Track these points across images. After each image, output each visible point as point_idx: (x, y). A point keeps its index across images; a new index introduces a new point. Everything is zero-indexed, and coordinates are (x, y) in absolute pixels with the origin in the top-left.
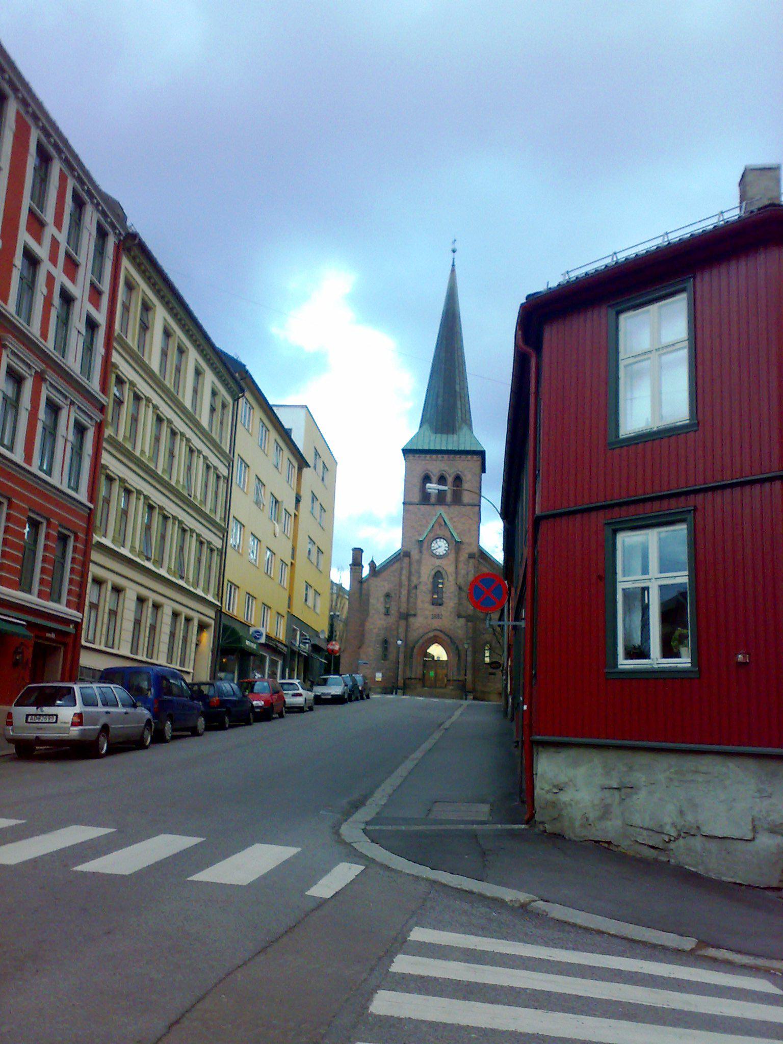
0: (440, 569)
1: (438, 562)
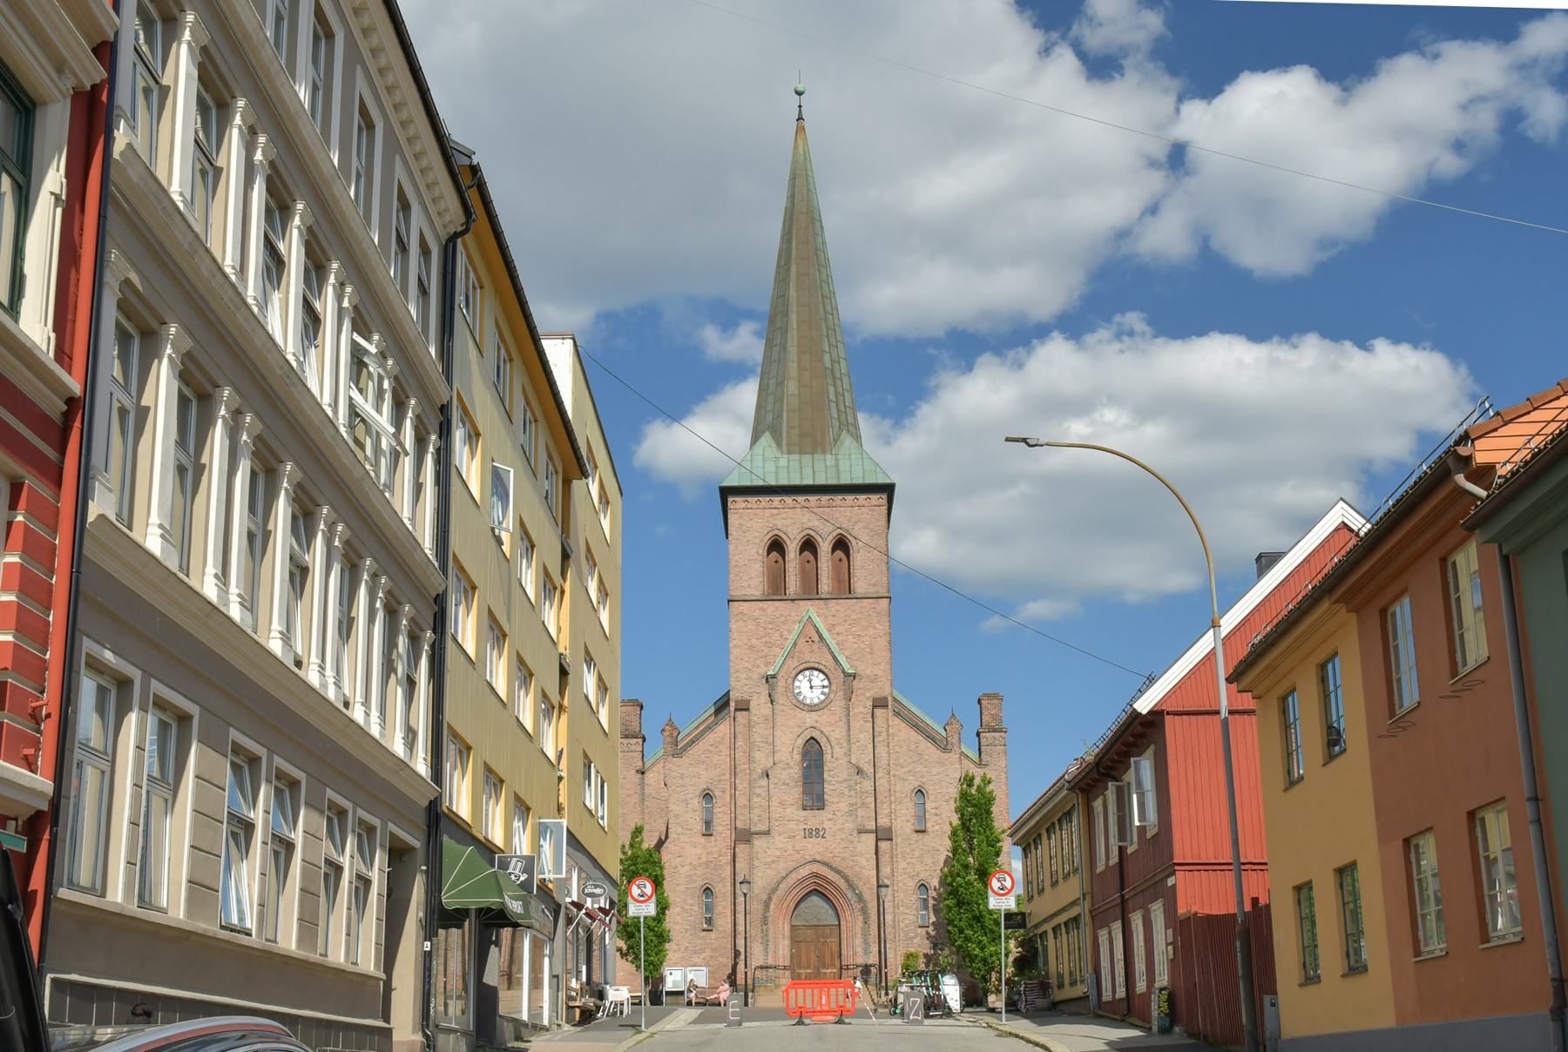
0: (816, 734)
1: (810, 719)
